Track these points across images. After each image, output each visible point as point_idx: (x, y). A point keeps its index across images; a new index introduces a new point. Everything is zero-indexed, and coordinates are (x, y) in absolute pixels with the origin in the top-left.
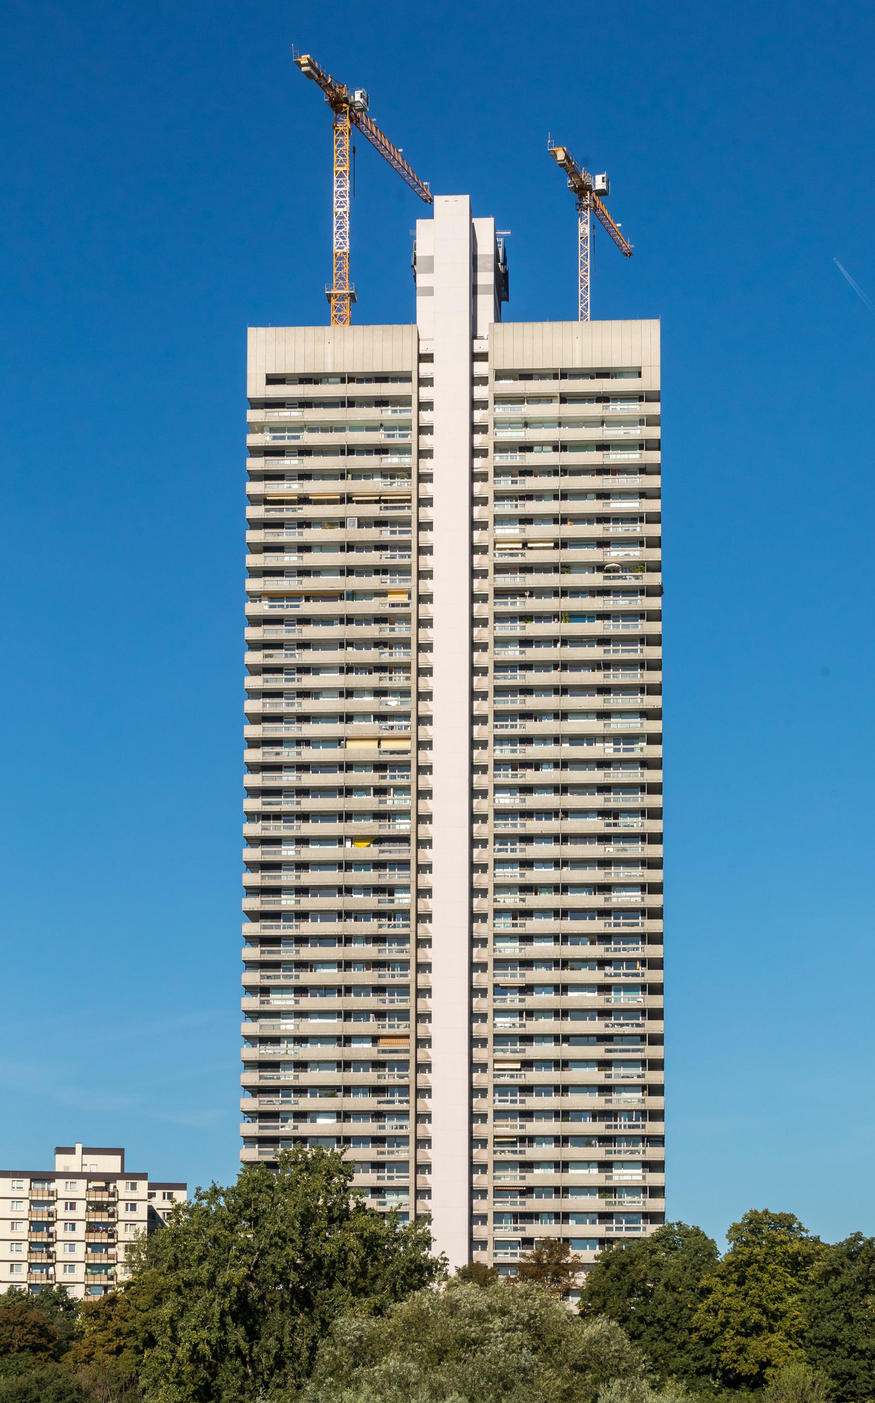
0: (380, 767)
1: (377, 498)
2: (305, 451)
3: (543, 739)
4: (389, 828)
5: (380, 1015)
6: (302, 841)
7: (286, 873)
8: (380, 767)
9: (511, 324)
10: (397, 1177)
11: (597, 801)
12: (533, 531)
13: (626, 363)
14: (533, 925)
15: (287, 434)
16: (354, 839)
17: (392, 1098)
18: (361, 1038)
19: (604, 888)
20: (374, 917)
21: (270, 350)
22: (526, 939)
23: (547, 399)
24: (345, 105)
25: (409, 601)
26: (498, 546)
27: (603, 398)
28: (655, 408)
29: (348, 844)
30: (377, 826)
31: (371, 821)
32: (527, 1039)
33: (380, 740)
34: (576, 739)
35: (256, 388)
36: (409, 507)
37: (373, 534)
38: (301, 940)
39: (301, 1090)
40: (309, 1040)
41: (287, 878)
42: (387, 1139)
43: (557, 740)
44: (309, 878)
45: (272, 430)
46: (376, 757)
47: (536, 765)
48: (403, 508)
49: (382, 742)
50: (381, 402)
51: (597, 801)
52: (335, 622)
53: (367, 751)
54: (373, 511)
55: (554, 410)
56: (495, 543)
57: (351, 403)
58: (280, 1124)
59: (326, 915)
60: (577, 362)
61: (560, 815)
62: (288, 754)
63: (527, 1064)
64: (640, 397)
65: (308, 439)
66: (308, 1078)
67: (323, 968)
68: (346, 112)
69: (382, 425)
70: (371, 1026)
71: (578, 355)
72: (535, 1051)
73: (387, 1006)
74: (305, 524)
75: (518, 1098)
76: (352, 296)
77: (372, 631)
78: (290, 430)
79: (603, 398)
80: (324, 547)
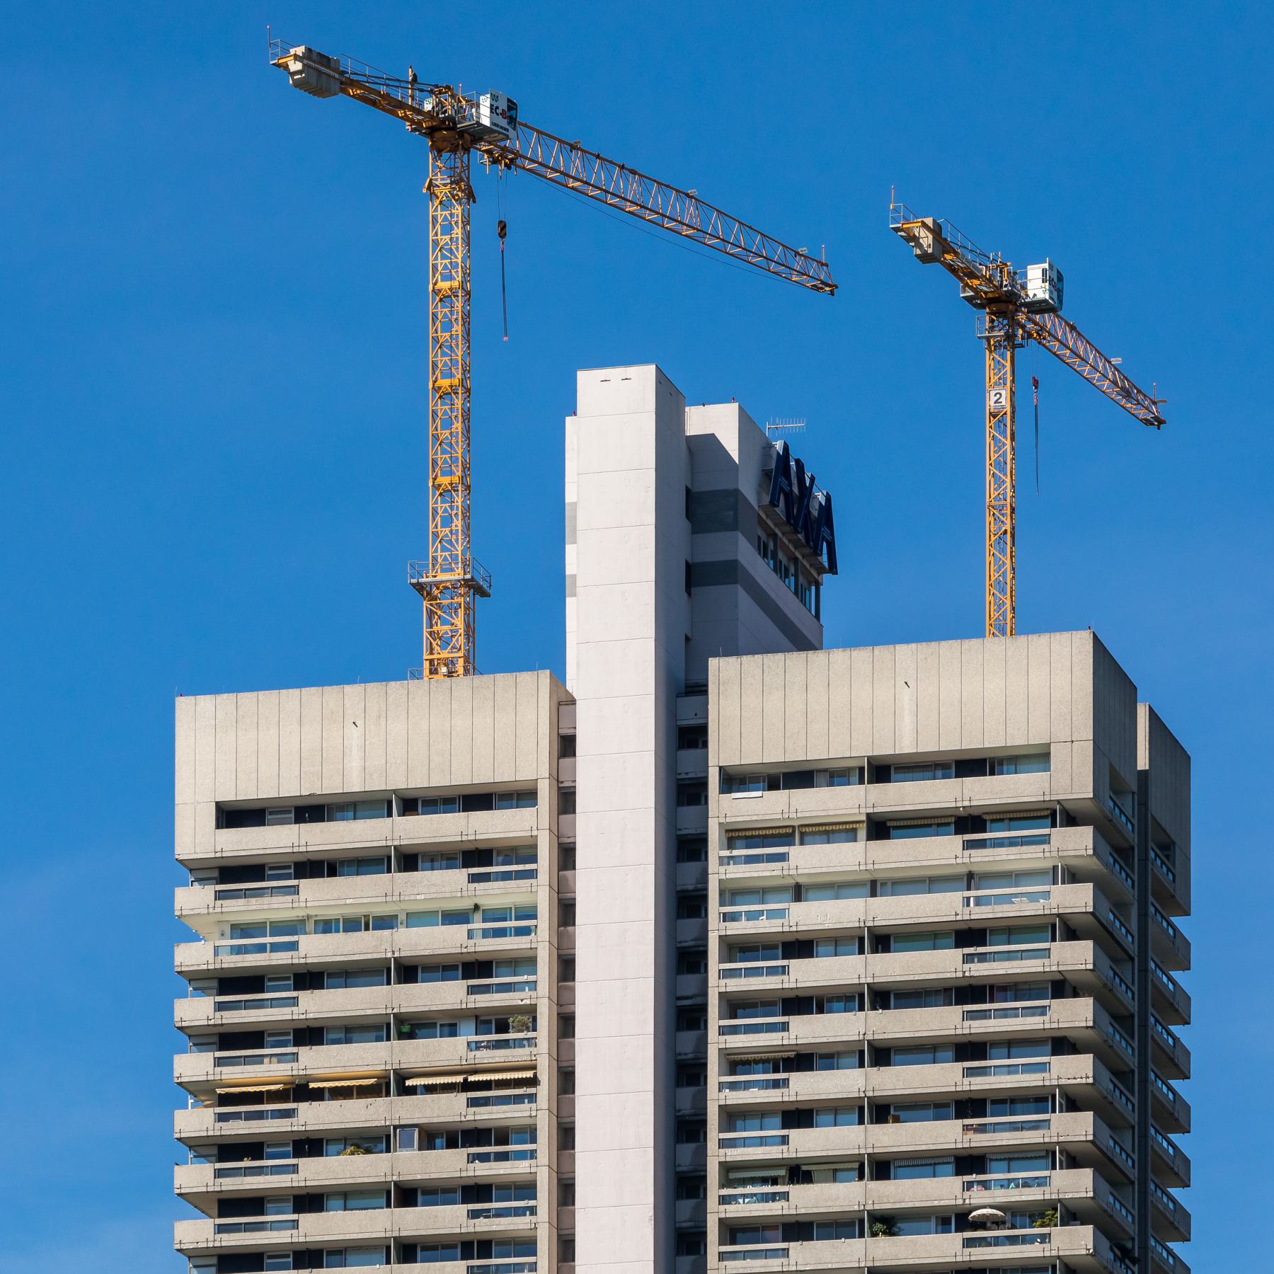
1: (460, 1079)
3: (837, 1110)
13: (1016, 737)
15: (268, 940)
21: (228, 745)
36: (532, 1098)
57: (409, 860)
65: (315, 949)
71: (907, 724)
74: (310, 1145)
80: (351, 1196)
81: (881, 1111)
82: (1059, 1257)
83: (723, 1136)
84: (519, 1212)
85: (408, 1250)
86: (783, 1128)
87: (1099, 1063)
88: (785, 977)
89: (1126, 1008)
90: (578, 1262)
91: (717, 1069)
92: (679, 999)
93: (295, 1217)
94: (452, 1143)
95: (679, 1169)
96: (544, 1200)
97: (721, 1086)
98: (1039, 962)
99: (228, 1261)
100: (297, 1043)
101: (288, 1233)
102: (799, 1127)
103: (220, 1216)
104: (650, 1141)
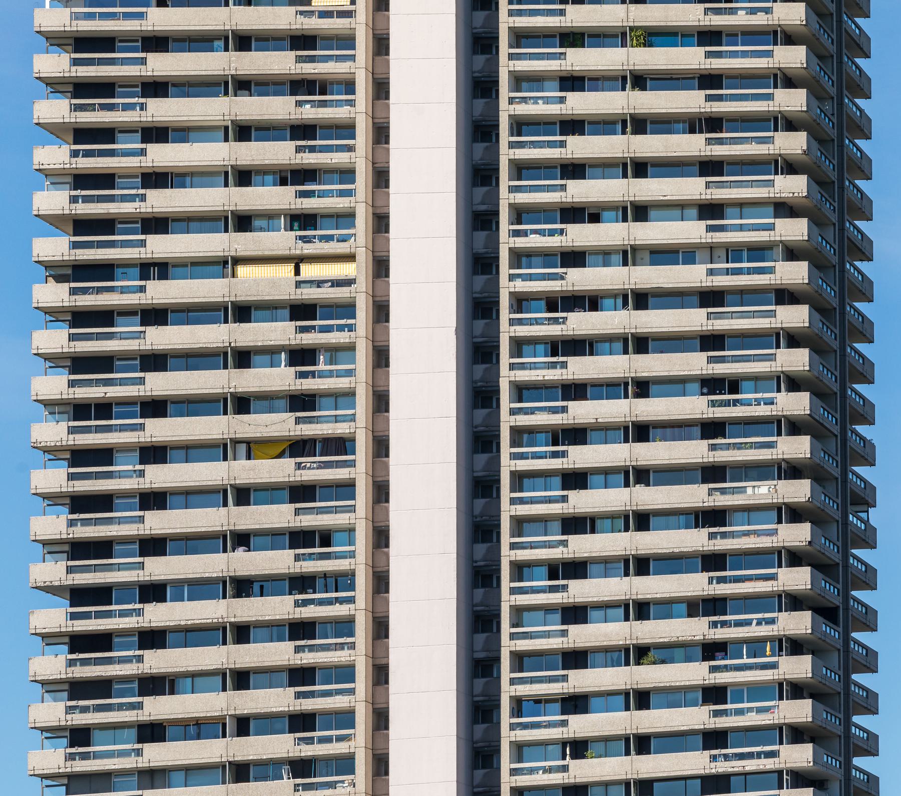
3: (605, 256)
8: (302, 312)
25: (352, 8)
33: (298, 261)
34: (663, 254)
47: (591, 301)
49: (304, 268)
53: (273, 282)
59: (200, 588)
81: (642, 565)
82: (780, 155)
83: (514, 585)
84: (341, 647)
85: (241, 772)
86: (563, 489)
87: (810, 95)
88: (565, 460)
89: (828, 135)
90: (392, 189)
91: (508, 486)
92: (476, 427)
93: (141, 513)
94: (283, 182)
95: (475, 474)
96: (361, 683)
97: (511, 101)
98: (767, 320)
99: (73, 781)
100: (145, 49)
101: (138, 67)
102: (575, 355)
103: (74, 235)
104: (454, 458)
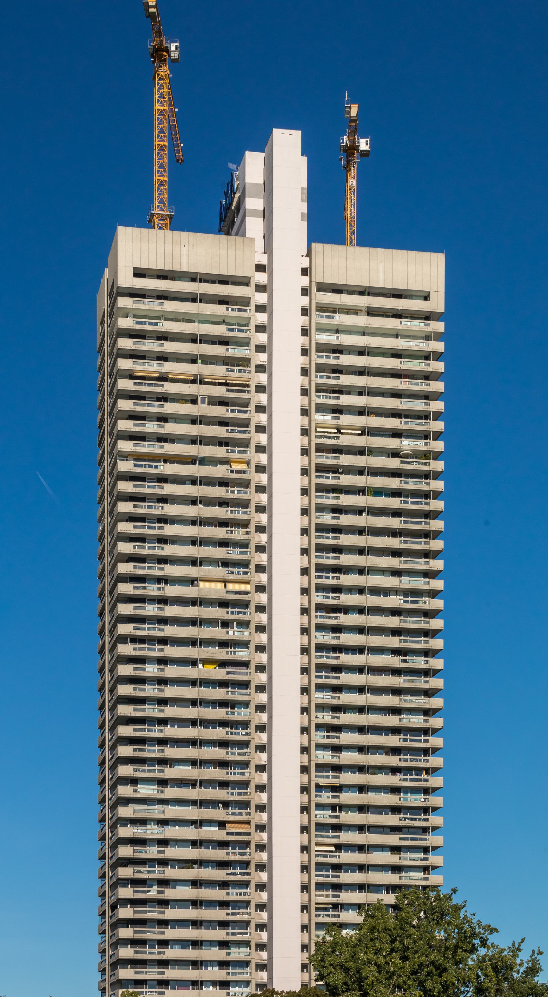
0: (223, 604)
1: (224, 381)
2: (163, 337)
4: (231, 654)
5: (226, 804)
6: (163, 661)
7: (149, 687)
8: (223, 604)
9: (329, 245)
10: (149, 932)
11: (394, 642)
12: (346, 420)
14: (346, 738)
16: (206, 662)
17: (234, 871)
18: (210, 823)
19: (396, 711)
20: (219, 726)
21: (136, 248)
22: (337, 749)
23: (355, 311)
24: (165, 53)
26: (318, 430)
27: (397, 315)
28: (439, 326)
29: (200, 666)
30: (225, 652)
31: (217, 648)
32: (337, 828)
34: (376, 591)
35: (126, 279)
37: (220, 411)
38: (163, 742)
39: (164, 863)
40: (170, 823)
41: (152, 691)
42: (231, 904)
43: (361, 591)
44: (170, 692)
45: (135, 316)
46: (223, 596)
48: (244, 391)
49: (228, 585)
50: (223, 301)
51: (394, 642)
52: (187, 482)
53: (217, 591)
54: (220, 392)
55: (361, 320)
56: (317, 427)
58: (147, 889)
60: (381, 283)
61: (366, 652)
62: (151, 590)
63: (339, 847)
64: (427, 317)
66: (171, 852)
67: (179, 765)
68: (165, 60)
69: (224, 321)
70: (219, 814)
71: (381, 277)
72: (347, 837)
73: (231, 798)
75: (331, 873)
76: (171, 217)
77: (220, 492)
78: (150, 317)
79: (397, 315)
